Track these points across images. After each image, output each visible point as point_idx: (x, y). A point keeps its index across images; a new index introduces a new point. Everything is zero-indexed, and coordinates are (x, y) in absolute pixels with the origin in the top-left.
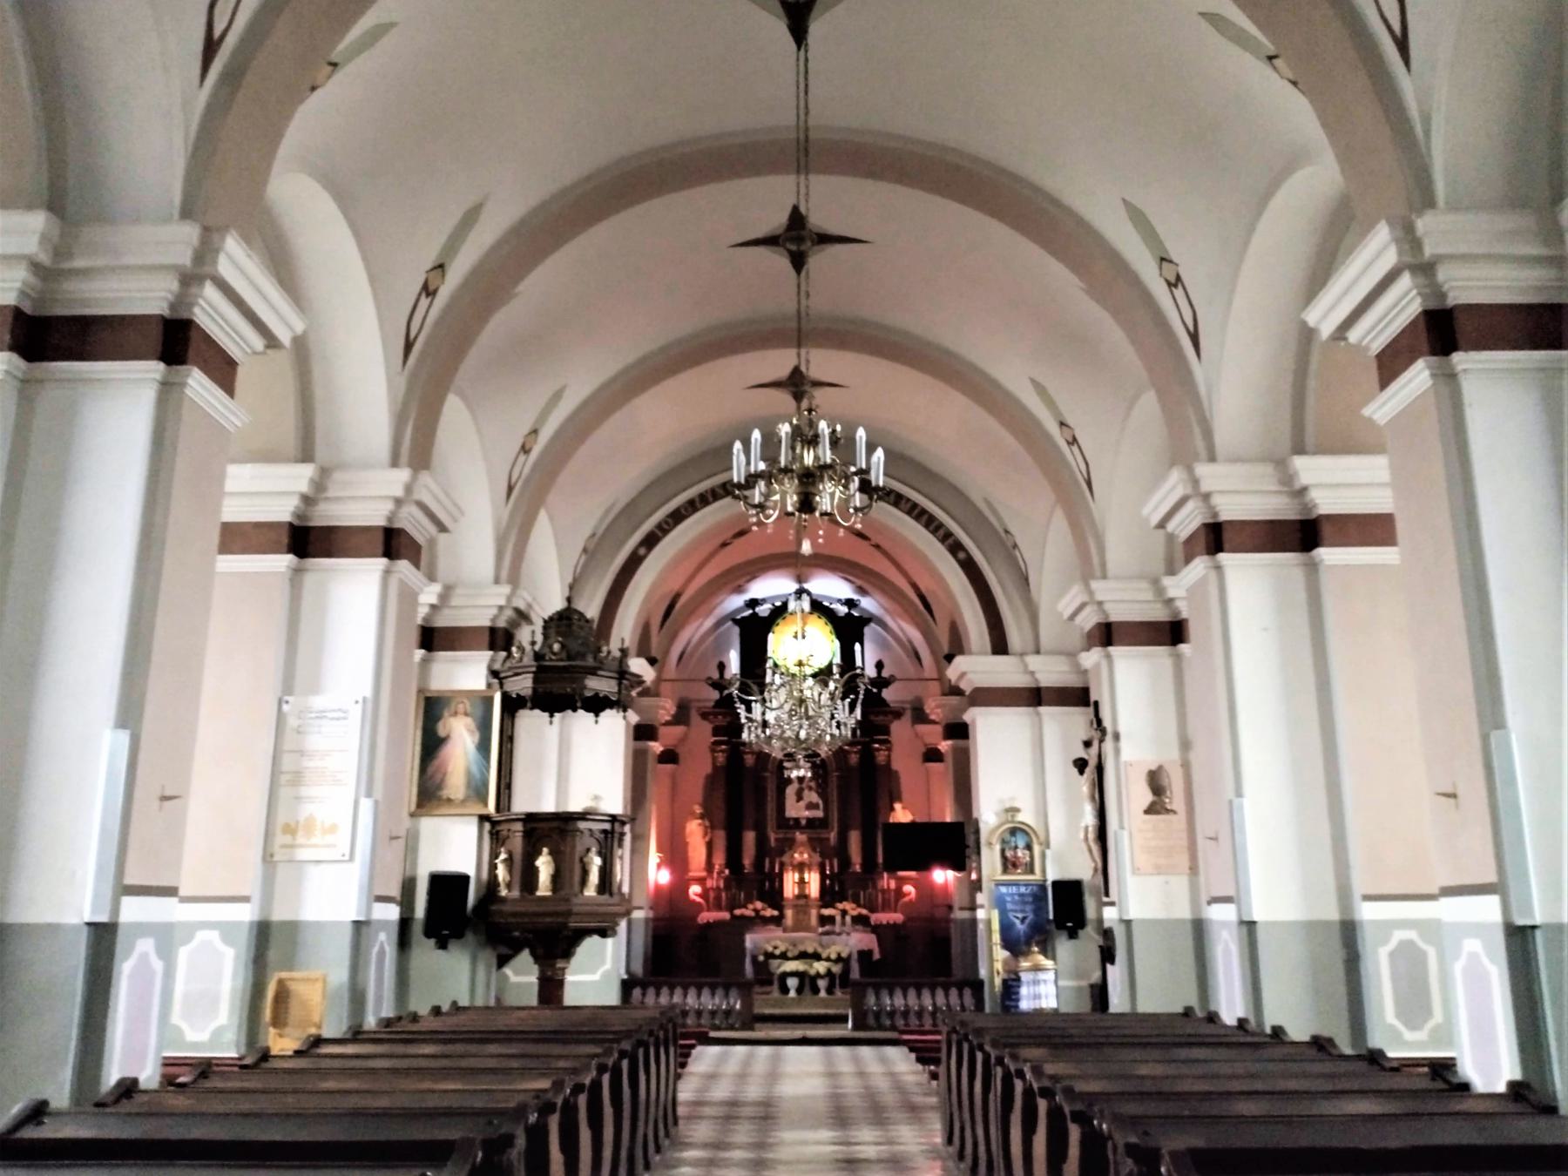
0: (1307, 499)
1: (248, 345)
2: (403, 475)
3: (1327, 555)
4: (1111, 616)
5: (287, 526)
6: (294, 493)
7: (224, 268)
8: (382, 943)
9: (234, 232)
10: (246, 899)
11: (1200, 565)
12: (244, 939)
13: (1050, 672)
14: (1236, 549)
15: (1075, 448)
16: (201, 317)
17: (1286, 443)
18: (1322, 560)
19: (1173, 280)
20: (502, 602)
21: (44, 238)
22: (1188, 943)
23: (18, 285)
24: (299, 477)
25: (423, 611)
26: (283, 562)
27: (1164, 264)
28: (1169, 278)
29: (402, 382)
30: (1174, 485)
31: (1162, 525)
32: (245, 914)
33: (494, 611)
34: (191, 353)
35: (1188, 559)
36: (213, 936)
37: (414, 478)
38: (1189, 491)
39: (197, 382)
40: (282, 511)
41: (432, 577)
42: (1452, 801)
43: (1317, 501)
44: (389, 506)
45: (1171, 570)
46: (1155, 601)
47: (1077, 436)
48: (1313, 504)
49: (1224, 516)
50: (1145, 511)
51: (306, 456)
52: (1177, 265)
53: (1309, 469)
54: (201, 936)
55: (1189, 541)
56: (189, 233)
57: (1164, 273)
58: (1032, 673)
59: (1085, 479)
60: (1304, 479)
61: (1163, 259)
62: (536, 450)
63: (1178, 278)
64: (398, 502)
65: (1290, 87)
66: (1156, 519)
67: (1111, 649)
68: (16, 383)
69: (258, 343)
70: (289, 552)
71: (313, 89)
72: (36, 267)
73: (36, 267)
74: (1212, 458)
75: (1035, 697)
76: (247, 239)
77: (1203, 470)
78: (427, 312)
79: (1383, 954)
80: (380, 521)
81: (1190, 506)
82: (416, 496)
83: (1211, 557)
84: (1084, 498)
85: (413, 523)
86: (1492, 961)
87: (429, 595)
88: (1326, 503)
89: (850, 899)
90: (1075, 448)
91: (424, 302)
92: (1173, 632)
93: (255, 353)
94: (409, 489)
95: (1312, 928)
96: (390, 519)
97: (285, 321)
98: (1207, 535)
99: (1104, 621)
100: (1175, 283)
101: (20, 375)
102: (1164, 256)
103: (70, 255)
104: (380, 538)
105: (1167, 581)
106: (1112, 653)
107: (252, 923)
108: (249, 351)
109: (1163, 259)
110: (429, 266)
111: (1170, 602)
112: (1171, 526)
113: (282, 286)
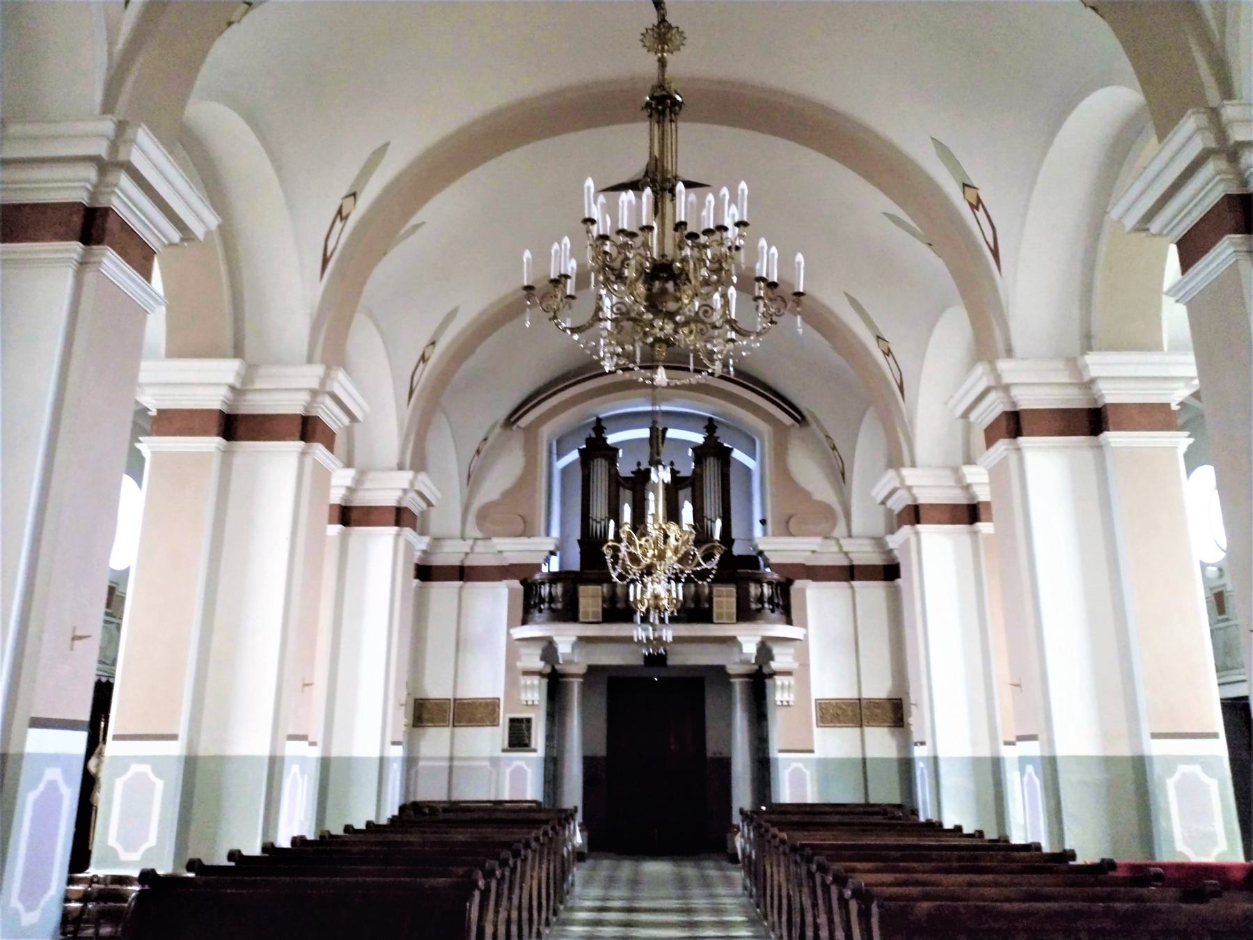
0: (1094, 391)
1: (165, 236)
2: (318, 370)
3: (1111, 438)
4: (1019, 403)
5: (217, 414)
6: (342, 486)
7: (137, 159)
8: (295, 774)
9: (144, 126)
10: (174, 737)
11: (906, 530)
12: (176, 774)
13: (865, 554)
14: (1033, 433)
15: (890, 359)
16: (117, 205)
17: (959, 458)
18: (1109, 443)
19: (886, 351)
20: (406, 486)
21: (238, 374)
22: (860, 768)
23: (341, 496)
24: (227, 370)
25: (418, 554)
26: (213, 443)
27: (966, 188)
28: (971, 201)
29: (407, 413)
30: (980, 378)
31: (883, 503)
32: (175, 749)
33: (400, 493)
34: (107, 239)
35: (899, 526)
36: (146, 768)
37: (415, 478)
38: (993, 383)
39: (110, 262)
40: (214, 400)
41: (349, 464)
42: (1018, 688)
43: (1104, 392)
44: (305, 397)
45: (891, 531)
46: (955, 487)
47: (982, 197)
48: (1099, 394)
49: (921, 501)
50: (873, 493)
51: (238, 351)
52: (977, 189)
53: (1097, 364)
54: (135, 768)
55: (899, 515)
56: (108, 126)
57: (967, 195)
58: (846, 554)
59: (990, 248)
60: (969, 479)
61: (965, 185)
62: (357, 212)
63: (979, 200)
64: (314, 393)
65: (1093, 13)
66: (880, 498)
67: (919, 526)
68: (220, 454)
69: (175, 236)
70: (218, 435)
71: (230, 24)
72: (232, 388)
73: (232, 388)
74: (913, 465)
75: (850, 573)
76: (155, 130)
77: (1003, 365)
78: (340, 234)
79: (1170, 783)
80: (298, 410)
81: (993, 396)
82: (417, 488)
83: (1012, 440)
84: (897, 401)
85: (415, 505)
86: (1038, 777)
87: (422, 543)
88: (1111, 395)
89: (440, 810)
90: (890, 359)
91: (338, 224)
92: (971, 513)
93: (171, 244)
94: (412, 483)
95: (976, 762)
96: (399, 502)
97: (202, 220)
98: (1008, 420)
99: (914, 503)
100: (888, 353)
101: (222, 449)
102: (966, 182)
103: (252, 382)
104: (298, 423)
105: (967, 470)
106: (1022, 445)
107: (318, 758)
108: (166, 242)
109: (965, 185)
110: (345, 192)
111: (967, 488)
112: (889, 504)
113: (214, 209)
